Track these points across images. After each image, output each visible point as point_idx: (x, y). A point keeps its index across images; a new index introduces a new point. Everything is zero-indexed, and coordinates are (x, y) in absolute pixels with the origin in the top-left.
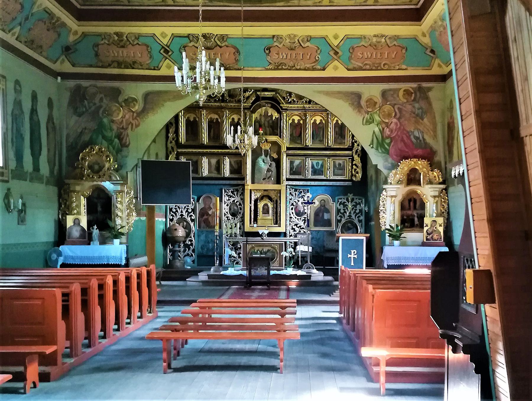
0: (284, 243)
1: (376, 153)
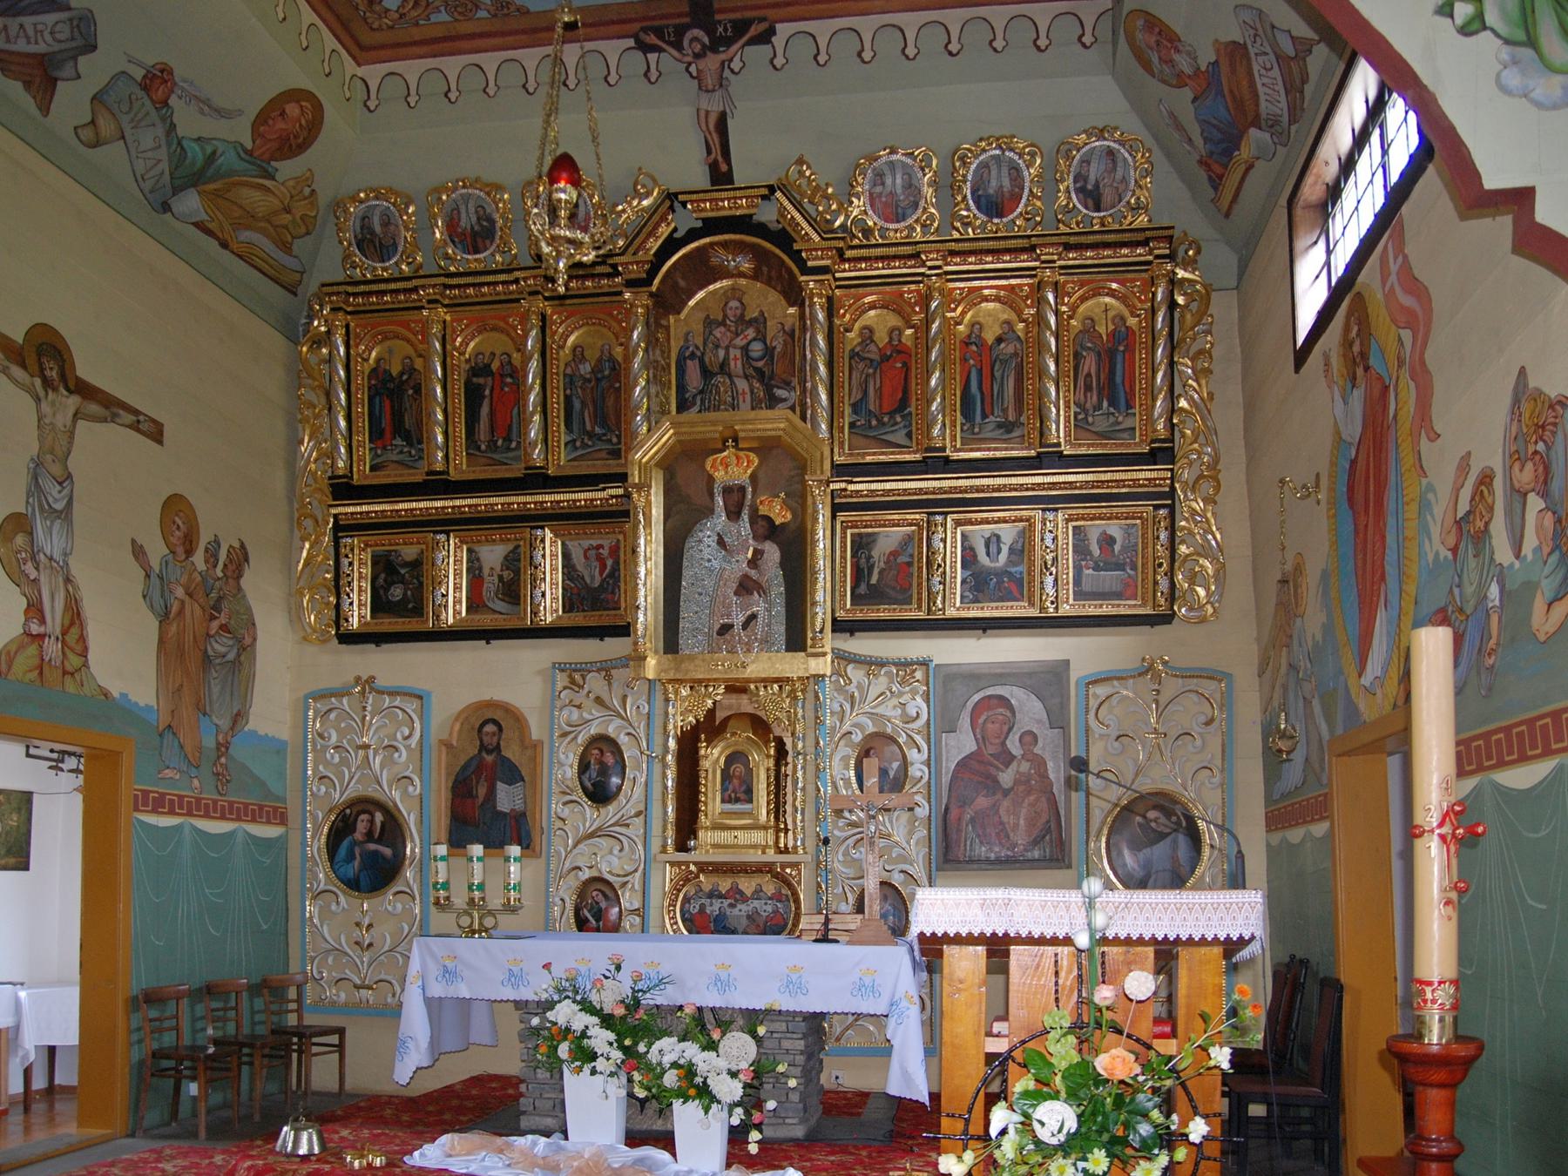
0: (1071, 525)
1: (1513, 79)
